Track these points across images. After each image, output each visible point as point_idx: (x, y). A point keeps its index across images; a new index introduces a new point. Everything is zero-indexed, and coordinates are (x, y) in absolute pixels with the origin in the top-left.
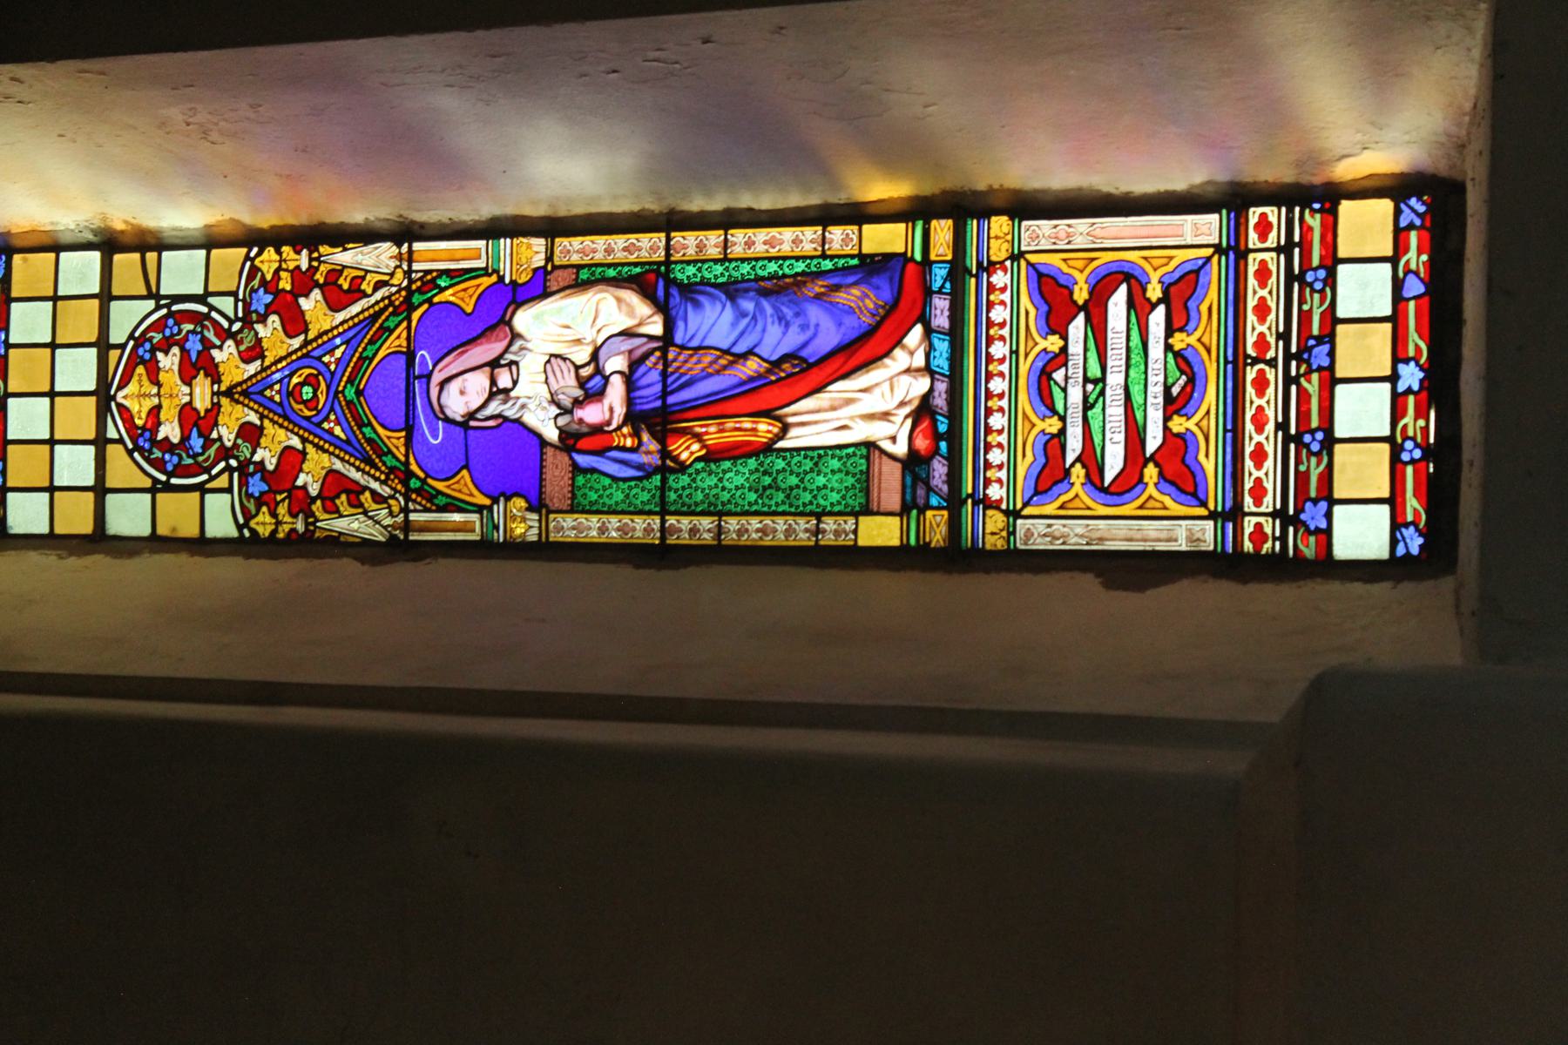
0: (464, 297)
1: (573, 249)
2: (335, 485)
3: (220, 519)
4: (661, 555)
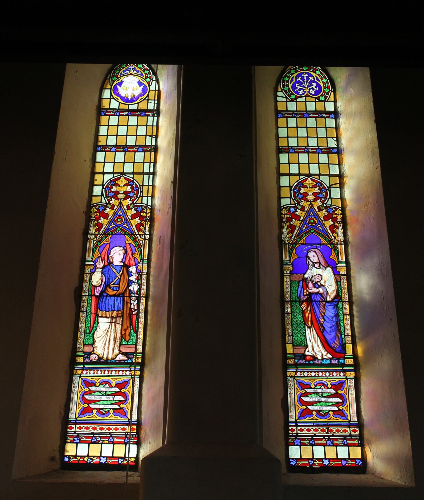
0: (333, 256)
1: (344, 280)
2: (293, 227)
3: (285, 202)
4: (282, 301)
